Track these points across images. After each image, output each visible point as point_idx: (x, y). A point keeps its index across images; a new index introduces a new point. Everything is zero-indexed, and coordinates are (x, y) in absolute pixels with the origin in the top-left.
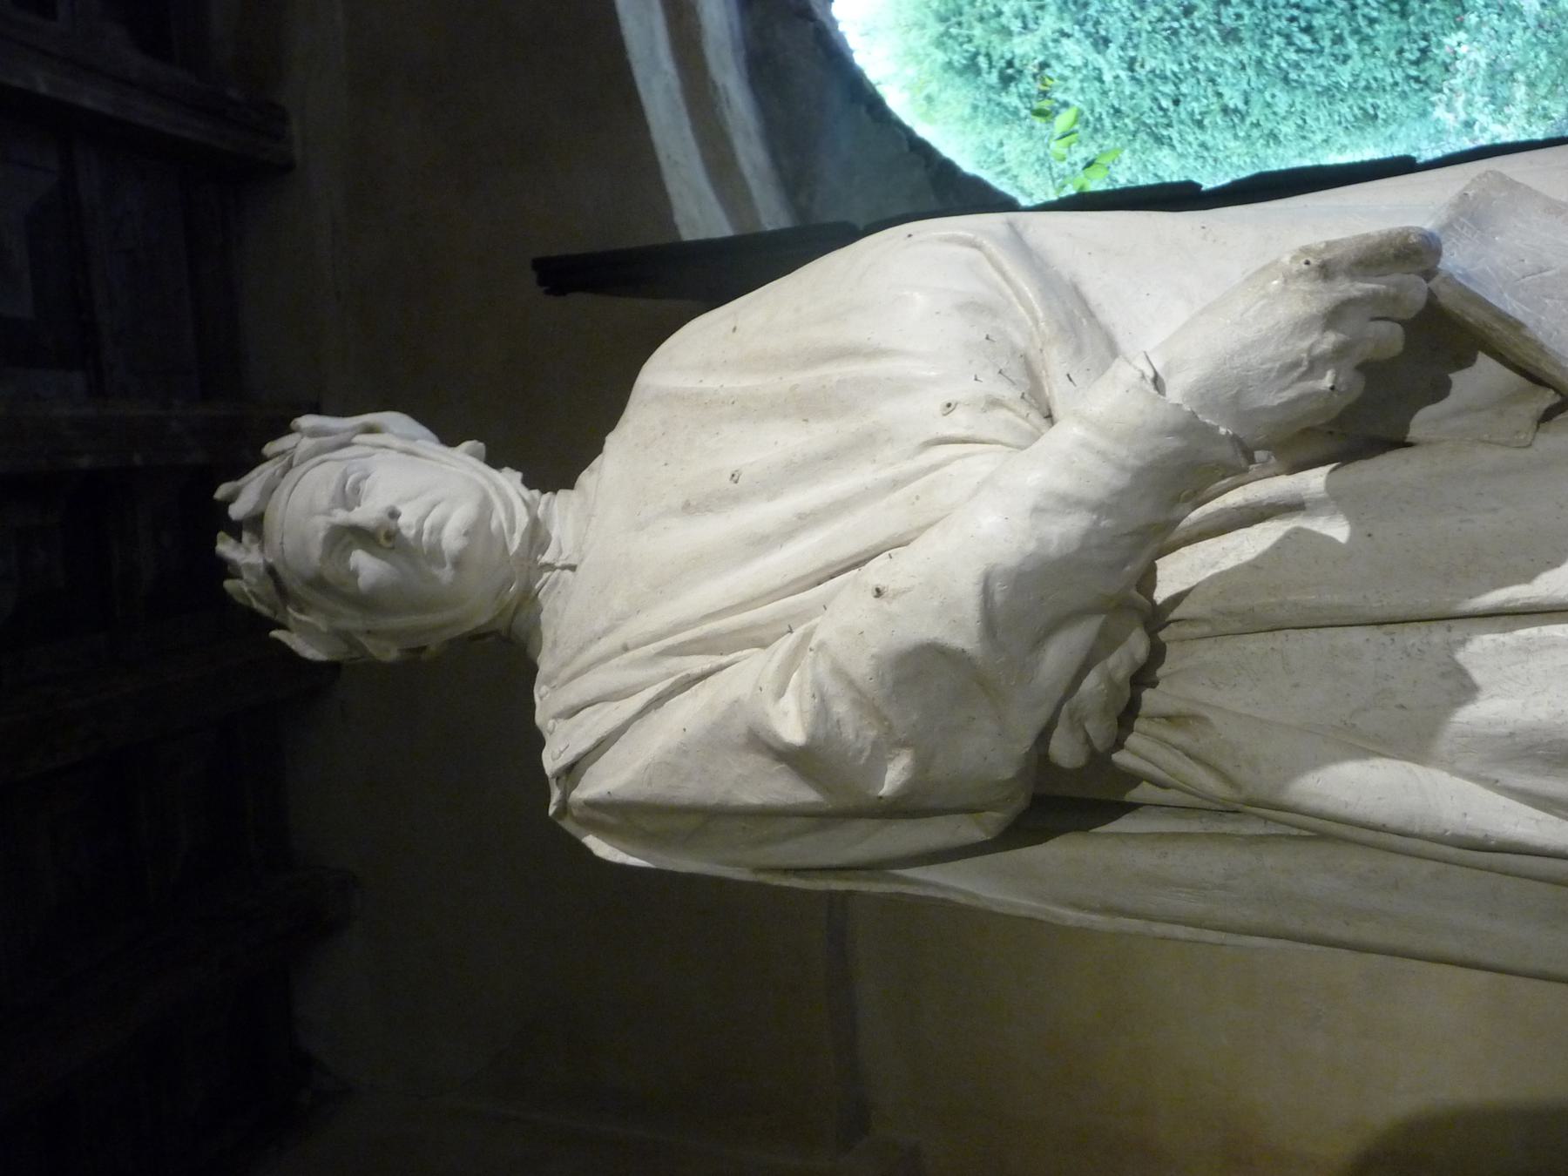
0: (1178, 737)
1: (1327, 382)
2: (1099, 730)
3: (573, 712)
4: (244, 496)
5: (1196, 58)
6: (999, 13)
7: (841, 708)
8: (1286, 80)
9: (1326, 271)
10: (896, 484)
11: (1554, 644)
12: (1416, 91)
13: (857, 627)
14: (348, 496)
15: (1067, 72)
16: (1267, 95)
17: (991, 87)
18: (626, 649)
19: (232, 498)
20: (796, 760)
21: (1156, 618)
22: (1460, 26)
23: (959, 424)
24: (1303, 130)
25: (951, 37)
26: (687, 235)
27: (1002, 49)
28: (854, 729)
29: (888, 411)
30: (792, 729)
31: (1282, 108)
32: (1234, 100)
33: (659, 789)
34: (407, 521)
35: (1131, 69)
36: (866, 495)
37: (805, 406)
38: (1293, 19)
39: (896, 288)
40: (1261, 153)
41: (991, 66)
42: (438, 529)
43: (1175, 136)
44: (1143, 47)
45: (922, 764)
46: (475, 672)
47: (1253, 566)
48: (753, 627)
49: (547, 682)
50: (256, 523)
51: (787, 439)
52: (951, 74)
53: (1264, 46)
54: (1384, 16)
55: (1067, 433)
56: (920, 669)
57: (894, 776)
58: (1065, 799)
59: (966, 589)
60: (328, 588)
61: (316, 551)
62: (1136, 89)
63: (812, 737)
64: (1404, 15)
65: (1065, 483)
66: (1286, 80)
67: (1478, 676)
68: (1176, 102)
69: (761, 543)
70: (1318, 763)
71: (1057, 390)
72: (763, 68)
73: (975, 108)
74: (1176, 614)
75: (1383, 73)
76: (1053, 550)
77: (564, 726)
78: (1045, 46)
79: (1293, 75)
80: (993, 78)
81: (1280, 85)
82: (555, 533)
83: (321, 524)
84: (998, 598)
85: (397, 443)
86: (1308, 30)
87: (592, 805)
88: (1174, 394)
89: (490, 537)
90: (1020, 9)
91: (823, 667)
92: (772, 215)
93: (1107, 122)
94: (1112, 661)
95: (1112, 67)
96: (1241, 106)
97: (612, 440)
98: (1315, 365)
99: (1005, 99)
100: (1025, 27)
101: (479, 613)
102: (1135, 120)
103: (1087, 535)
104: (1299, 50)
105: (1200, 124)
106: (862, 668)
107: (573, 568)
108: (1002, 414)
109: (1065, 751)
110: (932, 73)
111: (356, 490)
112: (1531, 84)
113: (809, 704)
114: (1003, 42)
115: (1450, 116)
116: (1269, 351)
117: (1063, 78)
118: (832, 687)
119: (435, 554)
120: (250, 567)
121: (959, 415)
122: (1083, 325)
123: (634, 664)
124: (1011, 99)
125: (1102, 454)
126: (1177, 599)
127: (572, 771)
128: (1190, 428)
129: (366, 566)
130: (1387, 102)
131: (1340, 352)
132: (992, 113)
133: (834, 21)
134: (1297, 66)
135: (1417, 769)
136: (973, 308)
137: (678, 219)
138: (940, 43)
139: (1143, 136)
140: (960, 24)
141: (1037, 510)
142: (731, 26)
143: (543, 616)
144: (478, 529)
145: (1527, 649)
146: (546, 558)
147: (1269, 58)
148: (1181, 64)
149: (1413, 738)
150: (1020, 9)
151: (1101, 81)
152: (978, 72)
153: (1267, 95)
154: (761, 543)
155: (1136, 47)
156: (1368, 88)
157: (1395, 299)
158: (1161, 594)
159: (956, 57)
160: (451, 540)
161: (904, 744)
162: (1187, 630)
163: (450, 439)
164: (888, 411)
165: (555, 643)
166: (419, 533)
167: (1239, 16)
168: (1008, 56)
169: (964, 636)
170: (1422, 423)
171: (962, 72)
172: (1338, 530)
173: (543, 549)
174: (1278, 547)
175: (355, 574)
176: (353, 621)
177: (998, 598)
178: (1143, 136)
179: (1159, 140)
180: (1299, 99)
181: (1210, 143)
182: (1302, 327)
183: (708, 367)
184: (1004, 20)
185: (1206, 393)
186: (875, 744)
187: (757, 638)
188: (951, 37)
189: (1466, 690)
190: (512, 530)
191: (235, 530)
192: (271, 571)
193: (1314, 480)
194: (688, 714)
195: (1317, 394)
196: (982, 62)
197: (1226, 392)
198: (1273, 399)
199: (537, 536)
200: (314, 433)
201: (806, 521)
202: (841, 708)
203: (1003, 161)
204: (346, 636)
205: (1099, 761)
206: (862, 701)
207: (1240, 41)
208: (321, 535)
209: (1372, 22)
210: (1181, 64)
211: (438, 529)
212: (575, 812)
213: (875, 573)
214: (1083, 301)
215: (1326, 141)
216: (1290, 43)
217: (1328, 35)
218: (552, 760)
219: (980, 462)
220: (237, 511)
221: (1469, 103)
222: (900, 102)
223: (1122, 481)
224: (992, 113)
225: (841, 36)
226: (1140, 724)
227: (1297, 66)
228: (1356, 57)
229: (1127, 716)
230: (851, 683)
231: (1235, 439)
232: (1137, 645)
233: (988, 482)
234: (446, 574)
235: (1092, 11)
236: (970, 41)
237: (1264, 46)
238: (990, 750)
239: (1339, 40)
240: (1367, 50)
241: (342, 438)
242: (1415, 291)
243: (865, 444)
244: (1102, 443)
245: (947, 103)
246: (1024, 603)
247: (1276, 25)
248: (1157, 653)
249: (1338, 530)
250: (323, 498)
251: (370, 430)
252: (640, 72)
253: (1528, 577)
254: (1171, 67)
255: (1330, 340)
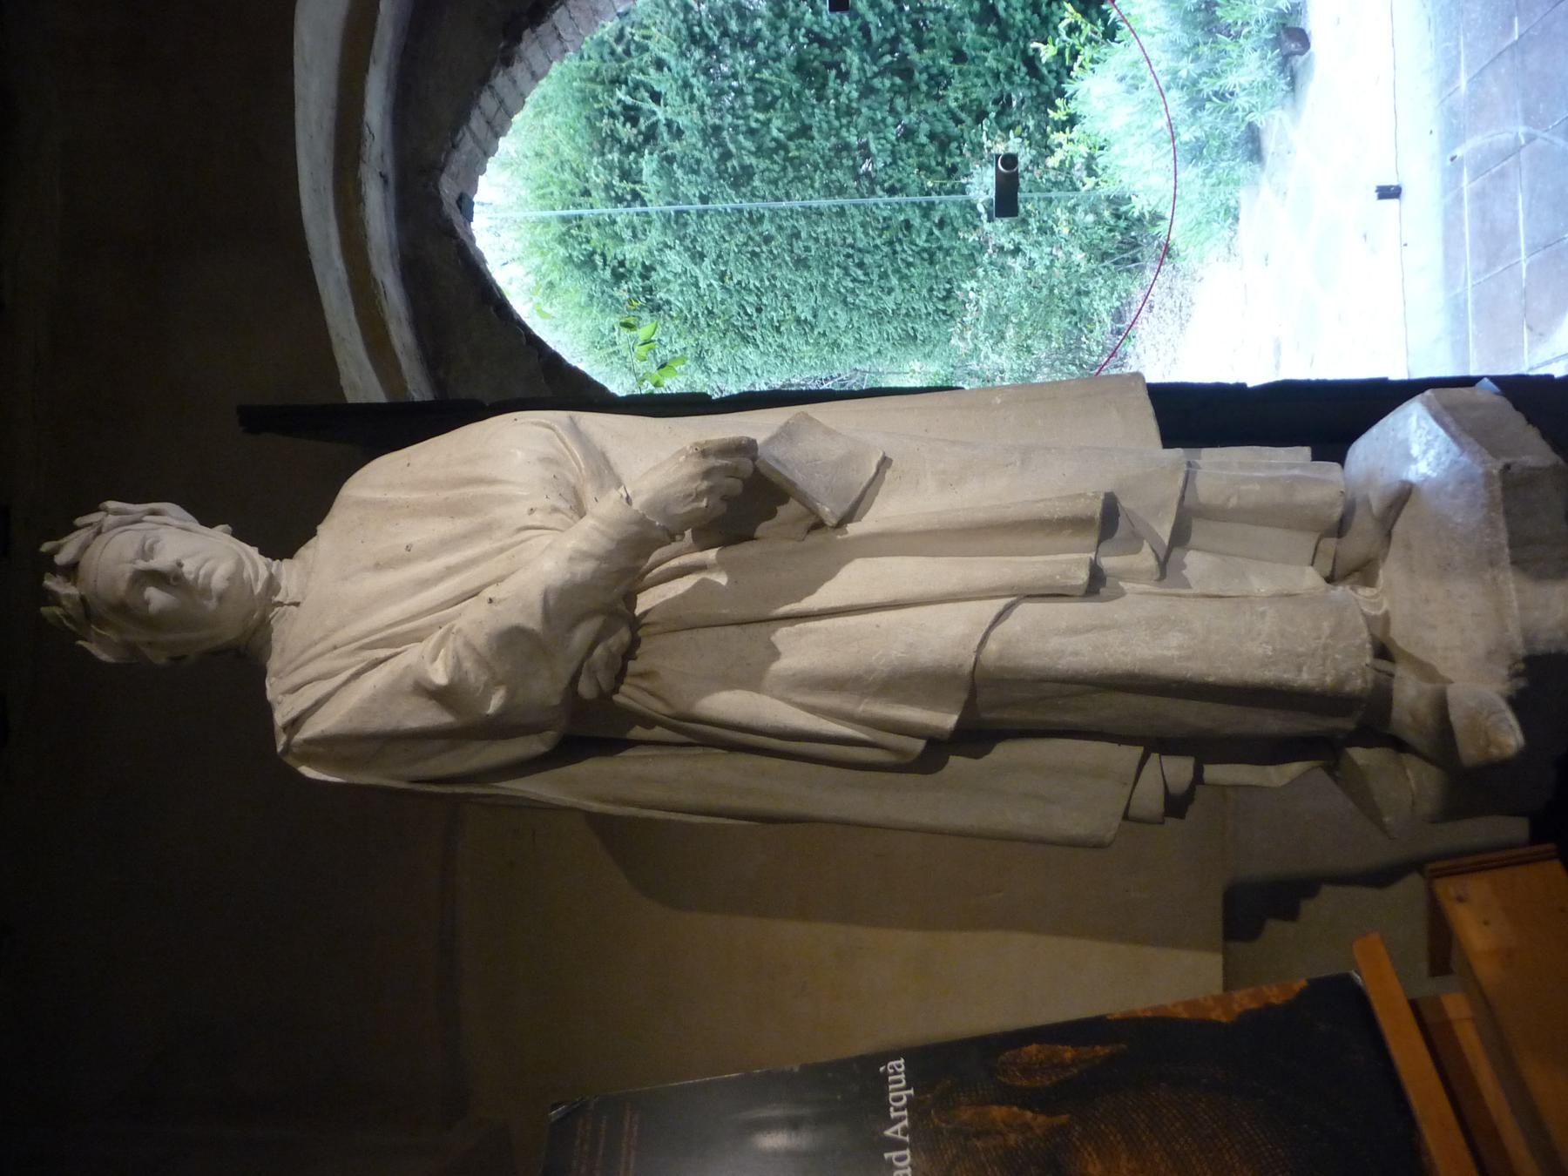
0: (645, 684)
1: (704, 504)
2: (604, 679)
3: (296, 689)
4: (67, 551)
5: (774, 277)
6: (614, 222)
7: (468, 665)
8: (845, 302)
9: (704, 453)
10: (502, 550)
11: (811, 631)
12: (944, 322)
13: (477, 621)
14: (146, 553)
15: (670, 277)
16: (830, 313)
17: (604, 281)
18: (335, 648)
19: (56, 551)
20: (441, 696)
21: (635, 623)
22: (974, 276)
23: (537, 519)
24: (859, 344)
25: (572, 236)
26: (351, 398)
27: (614, 252)
28: (475, 675)
29: (500, 512)
30: (439, 676)
31: (842, 324)
32: (806, 314)
33: (356, 725)
34: (189, 568)
35: (722, 279)
36: (486, 557)
37: (453, 510)
38: (848, 256)
39: (513, 448)
40: (828, 357)
41: (605, 264)
42: (209, 576)
43: (758, 338)
44: (732, 264)
45: (511, 695)
46: (229, 666)
47: (683, 596)
48: (417, 630)
49: (276, 675)
50: (71, 571)
51: (440, 527)
52: (571, 267)
53: (827, 274)
54: (918, 262)
55: (588, 522)
56: (511, 639)
57: (495, 702)
58: (592, 727)
59: (535, 596)
60: (126, 611)
61: (122, 586)
62: (727, 296)
63: (451, 680)
64: (932, 263)
65: (585, 546)
66: (845, 302)
67: (780, 648)
68: (759, 310)
69: (425, 583)
70: (709, 692)
71: (589, 504)
72: (413, 270)
73: (591, 297)
74: (645, 621)
75: (918, 305)
76: (578, 578)
77: (289, 698)
78: (651, 253)
79: (850, 299)
80: (607, 274)
81: (841, 305)
82: (283, 583)
83: (127, 570)
84: (551, 603)
85: (177, 523)
86: (861, 265)
87: (309, 742)
88: (636, 505)
89: (243, 582)
90: (631, 222)
91: (459, 642)
92: (418, 389)
93: (702, 321)
94: (611, 641)
95: (706, 277)
96: (810, 318)
97: (321, 528)
98: (699, 496)
99: (617, 294)
100: (635, 236)
101: (229, 633)
102: (725, 322)
103: (595, 572)
104: (854, 280)
105: (778, 330)
106: (480, 640)
107: (297, 604)
108: (560, 516)
109: (586, 689)
110: (555, 264)
111: (152, 549)
112: (1020, 325)
113: (451, 662)
114: (616, 246)
115: (961, 345)
116: (679, 488)
117: (666, 280)
118: (463, 653)
119: (206, 591)
120: (69, 596)
121: (537, 515)
122: (603, 470)
123: (340, 656)
124: (622, 293)
125: (603, 533)
126: (645, 613)
127: (295, 724)
128: (642, 521)
129: (156, 597)
130: (921, 327)
131: (710, 491)
132: (605, 303)
133: (472, 238)
134: (853, 291)
135: (756, 695)
136: (547, 461)
137: (344, 382)
138: (562, 240)
139: (731, 334)
140: (579, 227)
141: (571, 559)
142: (390, 236)
143: (274, 635)
144: (235, 577)
145: (800, 634)
146: (278, 598)
147: (831, 283)
148: (762, 281)
149: (752, 680)
150: (631, 222)
151: (697, 285)
152: (595, 268)
153: (830, 313)
154: (425, 583)
155: (726, 263)
156: (907, 315)
157: (736, 469)
158: (638, 612)
159: (575, 254)
160: (218, 582)
161: (501, 683)
162: (651, 630)
163: (208, 521)
164: (500, 512)
165: (283, 650)
166: (196, 578)
167: (807, 249)
168: (620, 257)
169: (534, 623)
170: (762, 529)
171: (579, 267)
172: (722, 579)
173: (276, 591)
174: (695, 587)
175: (147, 603)
176: (139, 636)
177: (551, 603)
178: (731, 334)
179: (746, 340)
180: (855, 319)
181: (788, 345)
182: (692, 478)
183: (390, 486)
184: (617, 228)
185: (651, 505)
186: (486, 685)
187: (416, 637)
188: (572, 236)
189: (775, 655)
190: (257, 579)
191: (55, 570)
192: (83, 599)
193: (711, 555)
194: (375, 680)
195: (699, 509)
196: (598, 259)
197: (660, 505)
198: (682, 509)
199: (272, 585)
200: (116, 512)
201: (450, 571)
202: (468, 665)
203: (615, 344)
204: (132, 648)
205: (605, 697)
206: (481, 661)
207: (808, 268)
208: (128, 575)
209: (909, 265)
210: (762, 281)
211: (209, 576)
212: (295, 750)
213: (488, 593)
214: (607, 461)
215: (879, 351)
216: (847, 274)
217: (876, 271)
218: (281, 717)
219: (546, 538)
220: (61, 559)
221: (975, 337)
222: (523, 306)
223: (612, 546)
224: (605, 303)
225: (480, 254)
226: (628, 680)
227: (853, 291)
228: (898, 291)
229: (620, 676)
230: (474, 649)
231: (664, 528)
232: (624, 635)
233: (550, 546)
234: (212, 605)
235: (690, 230)
236: (588, 241)
237: (827, 274)
238: (546, 688)
239: (884, 276)
240: (906, 286)
241: (137, 517)
242: (746, 465)
243: (486, 529)
244: (603, 528)
245: (567, 291)
246: (565, 605)
247: (836, 259)
248: (635, 642)
249: (722, 579)
250: (130, 553)
251: (154, 513)
252: (318, 268)
253: (799, 600)
254: (754, 282)
255: (704, 485)
